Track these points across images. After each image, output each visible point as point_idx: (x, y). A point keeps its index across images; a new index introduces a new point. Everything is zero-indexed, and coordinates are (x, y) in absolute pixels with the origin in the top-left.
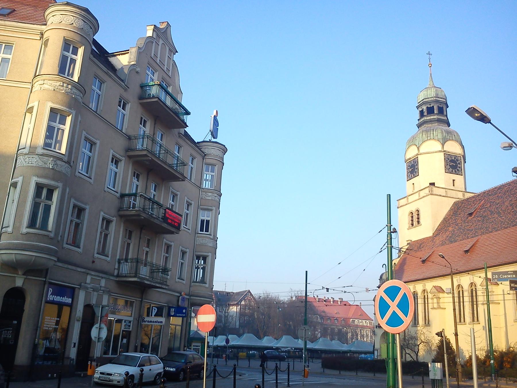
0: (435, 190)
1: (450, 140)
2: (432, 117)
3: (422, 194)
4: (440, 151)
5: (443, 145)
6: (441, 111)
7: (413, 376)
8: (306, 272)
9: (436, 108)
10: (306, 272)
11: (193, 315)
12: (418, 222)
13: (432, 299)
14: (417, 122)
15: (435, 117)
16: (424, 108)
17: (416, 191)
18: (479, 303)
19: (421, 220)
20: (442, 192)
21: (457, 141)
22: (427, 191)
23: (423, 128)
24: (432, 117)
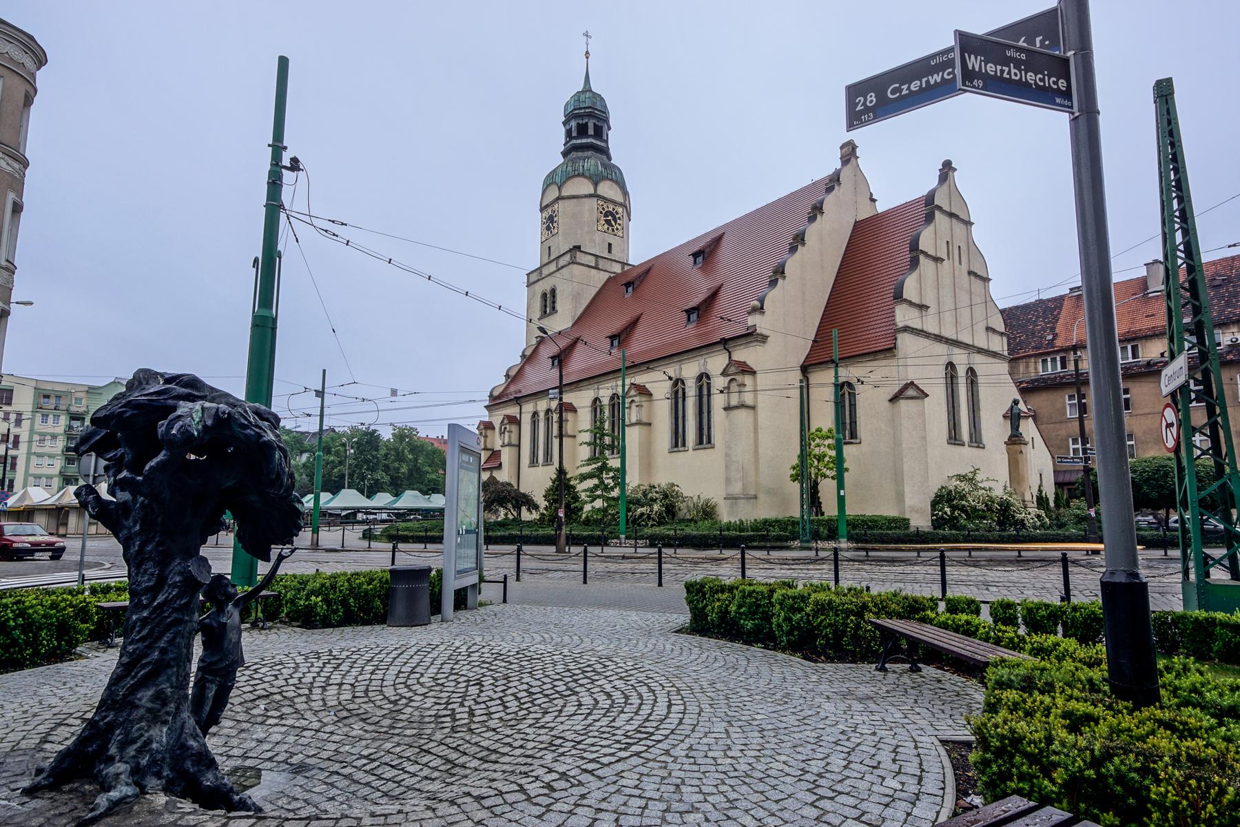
0: (581, 258)
1: (607, 179)
2: (584, 141)
3: (562, 262)
4: (591, 196)
5: (596, 185)
6: (599, 133)
7: (1041, 301)
8: (283, 63)
9: (591, 125)
10: (283, 63)
11: (192, 414)
12: (554, 308)
13: (350, 807)
14: (562, 148)
15: (589, 140)
16: (573, 124)
17: (552, 257)
18: (714, 391)
19: (558, 306)
20: (591, 261)
21: (616, 182)
22: (567, 258)
23: (574, 155)
24: (584, 141)
